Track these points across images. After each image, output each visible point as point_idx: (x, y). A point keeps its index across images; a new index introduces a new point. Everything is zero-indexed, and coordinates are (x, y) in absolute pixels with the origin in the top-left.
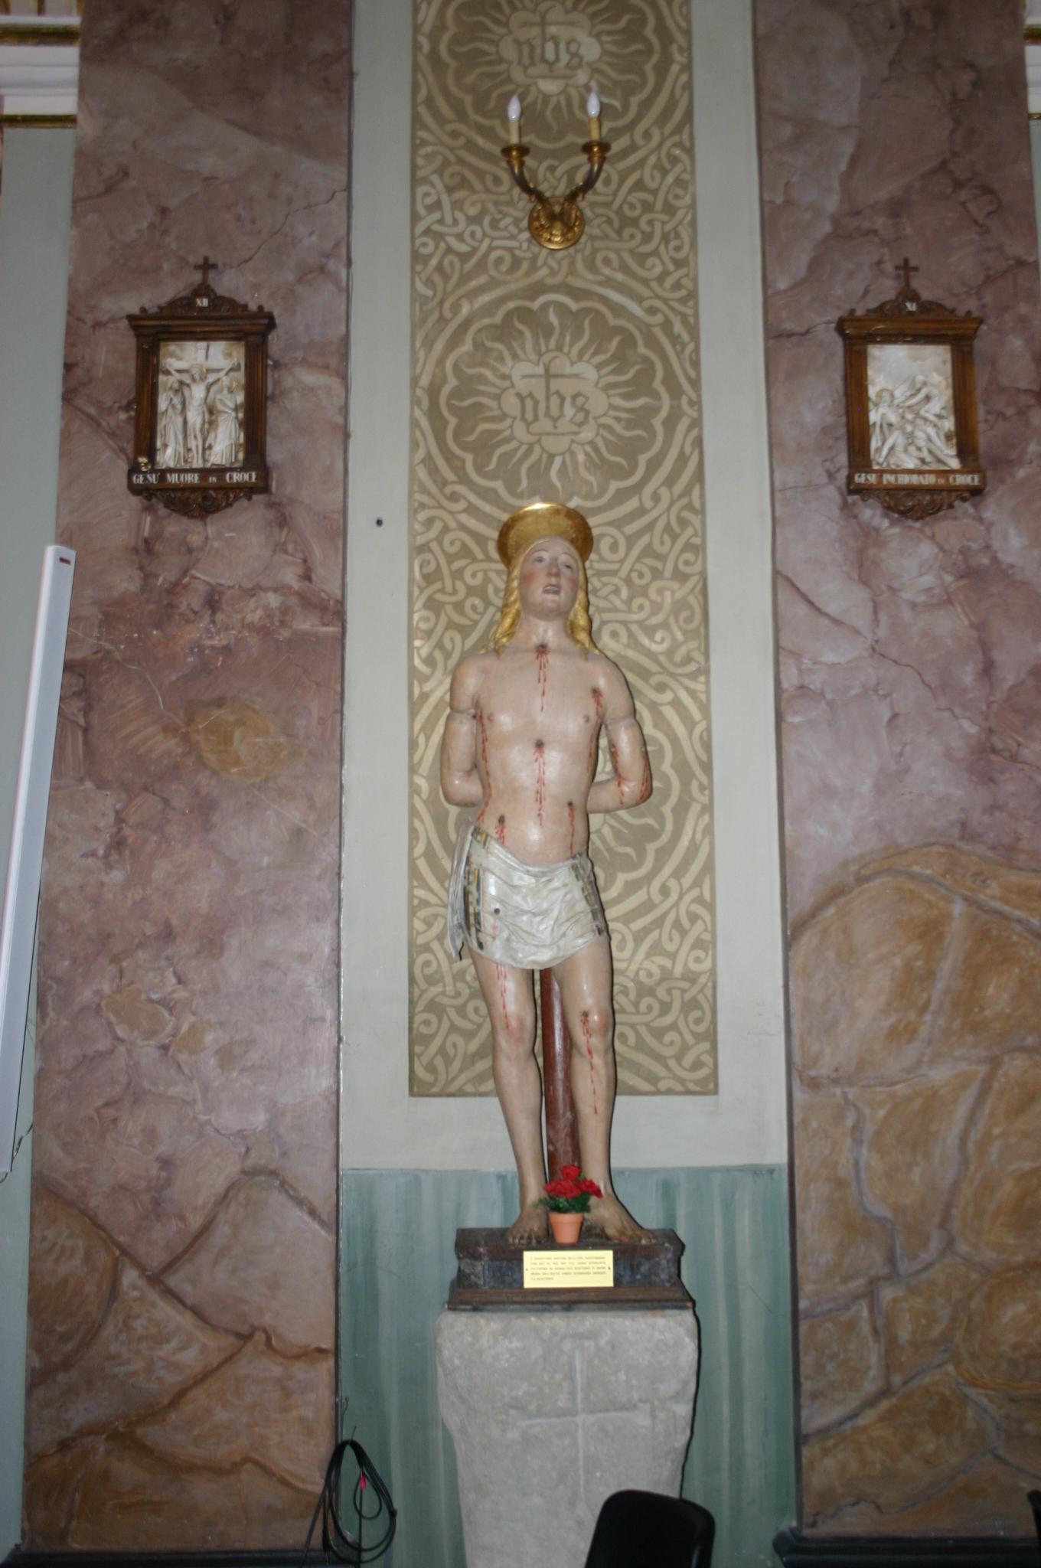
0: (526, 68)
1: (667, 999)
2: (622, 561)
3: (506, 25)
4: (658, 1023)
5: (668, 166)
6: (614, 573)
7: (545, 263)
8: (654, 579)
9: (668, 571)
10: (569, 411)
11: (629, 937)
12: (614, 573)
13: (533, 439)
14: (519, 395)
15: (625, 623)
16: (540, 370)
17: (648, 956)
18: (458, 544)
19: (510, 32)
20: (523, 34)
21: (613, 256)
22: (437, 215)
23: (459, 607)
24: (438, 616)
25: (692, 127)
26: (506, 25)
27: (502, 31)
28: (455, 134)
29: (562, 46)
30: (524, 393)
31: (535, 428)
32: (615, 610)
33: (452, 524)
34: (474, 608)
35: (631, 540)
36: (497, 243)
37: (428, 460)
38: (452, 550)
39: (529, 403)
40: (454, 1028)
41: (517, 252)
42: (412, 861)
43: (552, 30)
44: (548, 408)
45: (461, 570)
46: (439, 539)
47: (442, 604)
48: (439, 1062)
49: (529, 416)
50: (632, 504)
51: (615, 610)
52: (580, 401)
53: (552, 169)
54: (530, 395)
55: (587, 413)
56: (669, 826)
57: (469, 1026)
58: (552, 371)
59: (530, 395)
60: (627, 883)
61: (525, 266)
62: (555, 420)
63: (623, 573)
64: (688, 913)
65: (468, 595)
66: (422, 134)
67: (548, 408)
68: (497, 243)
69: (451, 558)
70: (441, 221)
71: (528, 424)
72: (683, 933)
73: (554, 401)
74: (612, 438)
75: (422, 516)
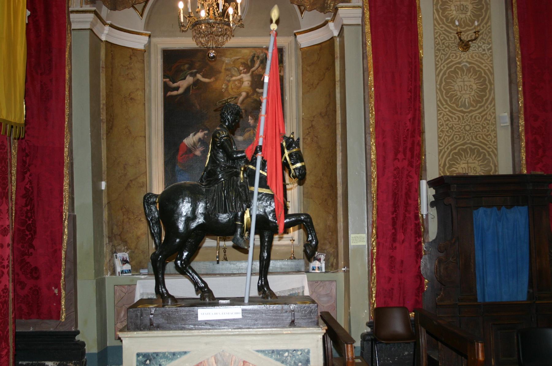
0: (460, 92)
1: (488, 129)
2: (481, 121)
3: (455, 82)
4: (487, 134)
5: (488, 34)
6: (479, 124)
7: (467, 138)
8: (487, 125)
9: (486, 42)
10: (469, 89)
11: (481, 117)
12: (479, 124)
13: (461, 95)
14: (458, 86)
15: (482, 134)
16: (466, 162)
17: (484, 121)
18: (447, 118)
19: (457, 84)
20: (459, 84)
21: (477, 55)
22: (439, 46)
23: (444, 50)
24: (443, 133)
25: (495, 101)
26: (455, 82)
27: (455, 83)
28: (442, 27)
29: (472, 169)
30: (463, 167)
31: (462, 93)
32: (479, 131)
33: (445, 114)
34: (447, 50)
35: (482, 117)
36: (452, 52)
37: (440, 101)
38: (445, 119)
39: (464, 169)
40: (446, 135)
41: (460, 135)
42: (436, 91)
43: (466, 83)
44: (464, 88)
45: (448, 124)
46: (443, 117)
47: (440, 50)
48: (443, 142)
49: (460, 90)
50: (482, 109)
51: (479, 131)
52: (475, 169)
53: (467, 116)
54: (464, 168)
55: (472, 89)
56: (484, 14)
57: (449, 135)
58: (469, 162)
59: (460, 86)
60: (480, 106)
61: (462, 138)
62: (462, 10)
63: (481, 124)
64: (489, 62)
65: (446, 48)
66: (435, 27)
67: (464, 88)
68: (452, 52)
69: (445, 121)
70: (440, 47)
71: (460, 92)
72: (487, 35)
73: (466, 87)
74: (482, 160)
75: (439, 112)
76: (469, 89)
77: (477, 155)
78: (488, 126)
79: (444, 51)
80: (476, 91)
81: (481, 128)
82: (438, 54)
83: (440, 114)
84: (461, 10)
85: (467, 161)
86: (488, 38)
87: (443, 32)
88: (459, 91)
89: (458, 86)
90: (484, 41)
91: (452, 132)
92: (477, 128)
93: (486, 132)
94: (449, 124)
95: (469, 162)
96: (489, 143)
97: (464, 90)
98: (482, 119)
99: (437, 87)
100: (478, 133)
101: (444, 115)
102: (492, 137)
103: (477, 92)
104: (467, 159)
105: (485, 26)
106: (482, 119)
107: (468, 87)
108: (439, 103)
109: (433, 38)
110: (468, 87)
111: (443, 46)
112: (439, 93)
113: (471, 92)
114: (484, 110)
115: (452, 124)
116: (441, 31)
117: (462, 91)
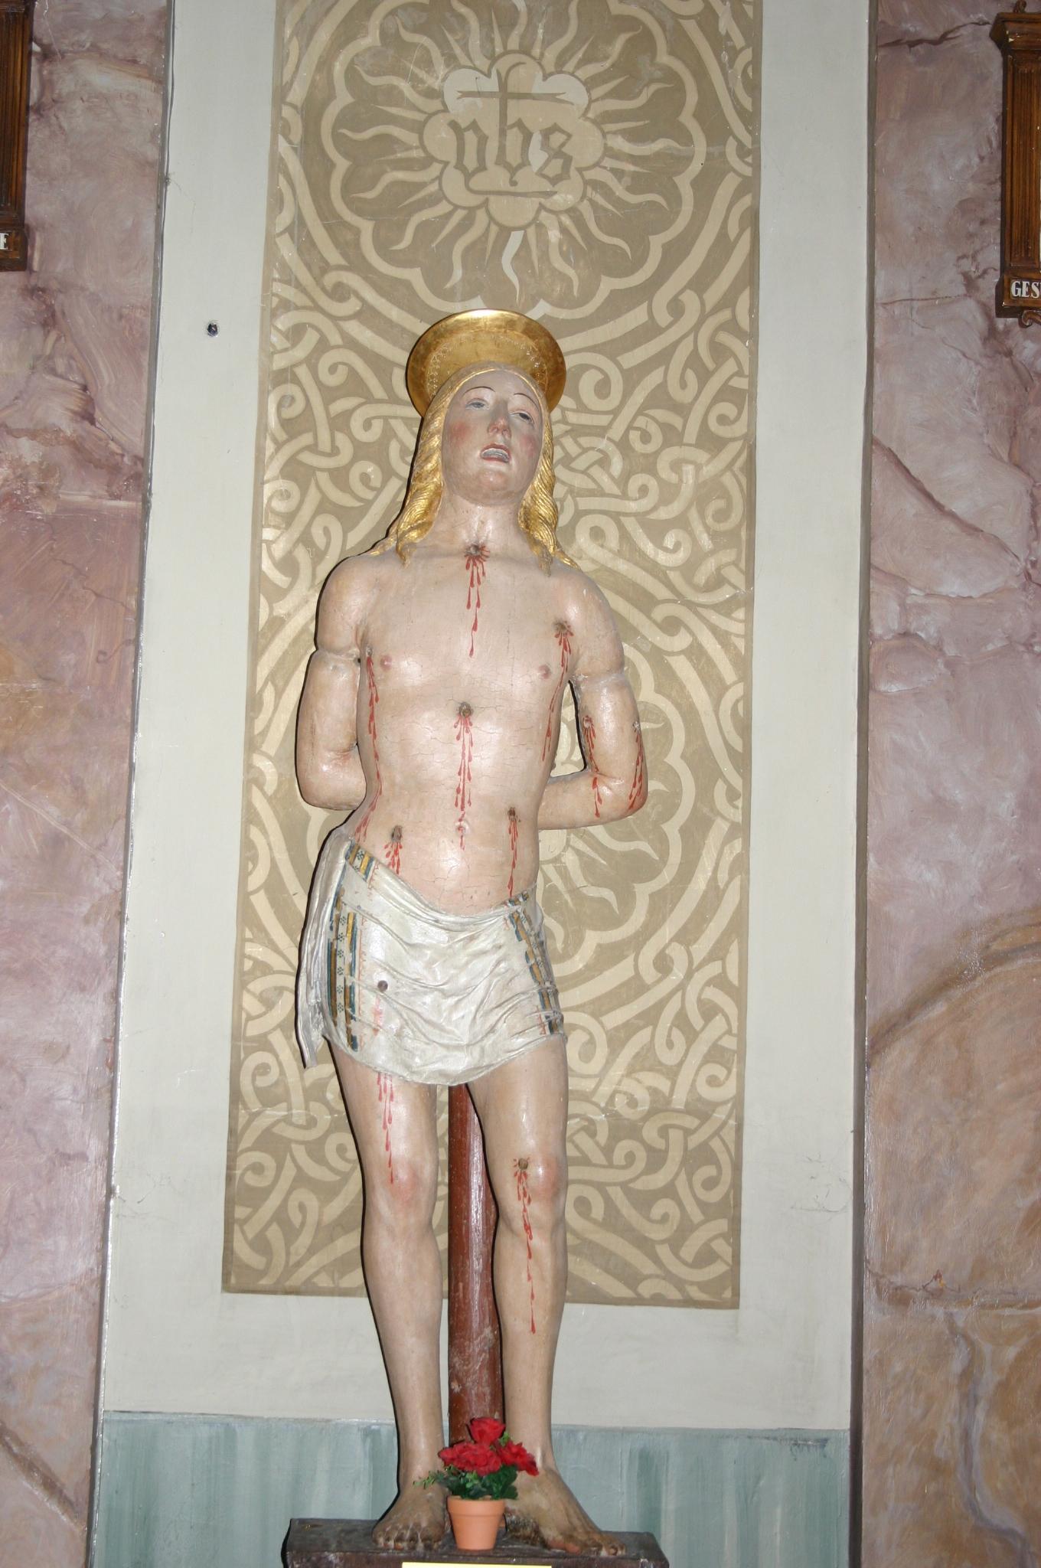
2: (615, 413)
6: (601, 431)
8: (667, 444)
11: (601, 1039)
12: (601, 431)
14: (454, 125)
17: (630, 1072)
18: (342, 371)
23: (339, 476)
31: (479, 182)
32: (600, 493)
33: (335, 339)
34: (365, 479)
35: (632, 378)
39: (471, 138)
40: (301, 1179)
44: (502, 149)
45: (347, 414)
47: (313, 470)
48: (275, 1234)
49: (471, 162)
50: (637, 317)
52: (557, 139)
54: (474, 126)
55: (568, 160)
62: (513, 170)
63: (616, 433)
64: (700, 1001)
65: (355, 459)
67: (502, 149)
71: (468, 176)
75: (284, 322)
76: (544, 156)
77: (579, 39)
78: (673, 453)
79: (320, 1160)
80: (598, 108)
81: (617, 465)
82: (270, 1173)
83: (295, 334)
84: (508, 166)
85: (503, 84)
86: (694, 1060)
87: (343, 334)
88: (460, 166)
89: (454, 125)
90: (677, 421)
91: (376, 479)
92: (581, 464)
93: (640, 1164)
94: (356, 424)
95: (512, 88)
96: (657, 1260)
97: (501, 160)
98: (627, 394)
99: (252, 780)
100: (584, 503)
101: (323, 345)
102: (695, 541)
103: (598, 186)
104: (503, 64)
105: (677, 952)
106: (627, 394)
107: (537, 139)
108: (287, 250)
109: (253, 376)
110: (537, 139)
111: (341, 439)
112: (294, 165)
113: (554, 181)
114: (650, 330)
115: (386, 419)
116: (334, 319)
117: (482, 167)
